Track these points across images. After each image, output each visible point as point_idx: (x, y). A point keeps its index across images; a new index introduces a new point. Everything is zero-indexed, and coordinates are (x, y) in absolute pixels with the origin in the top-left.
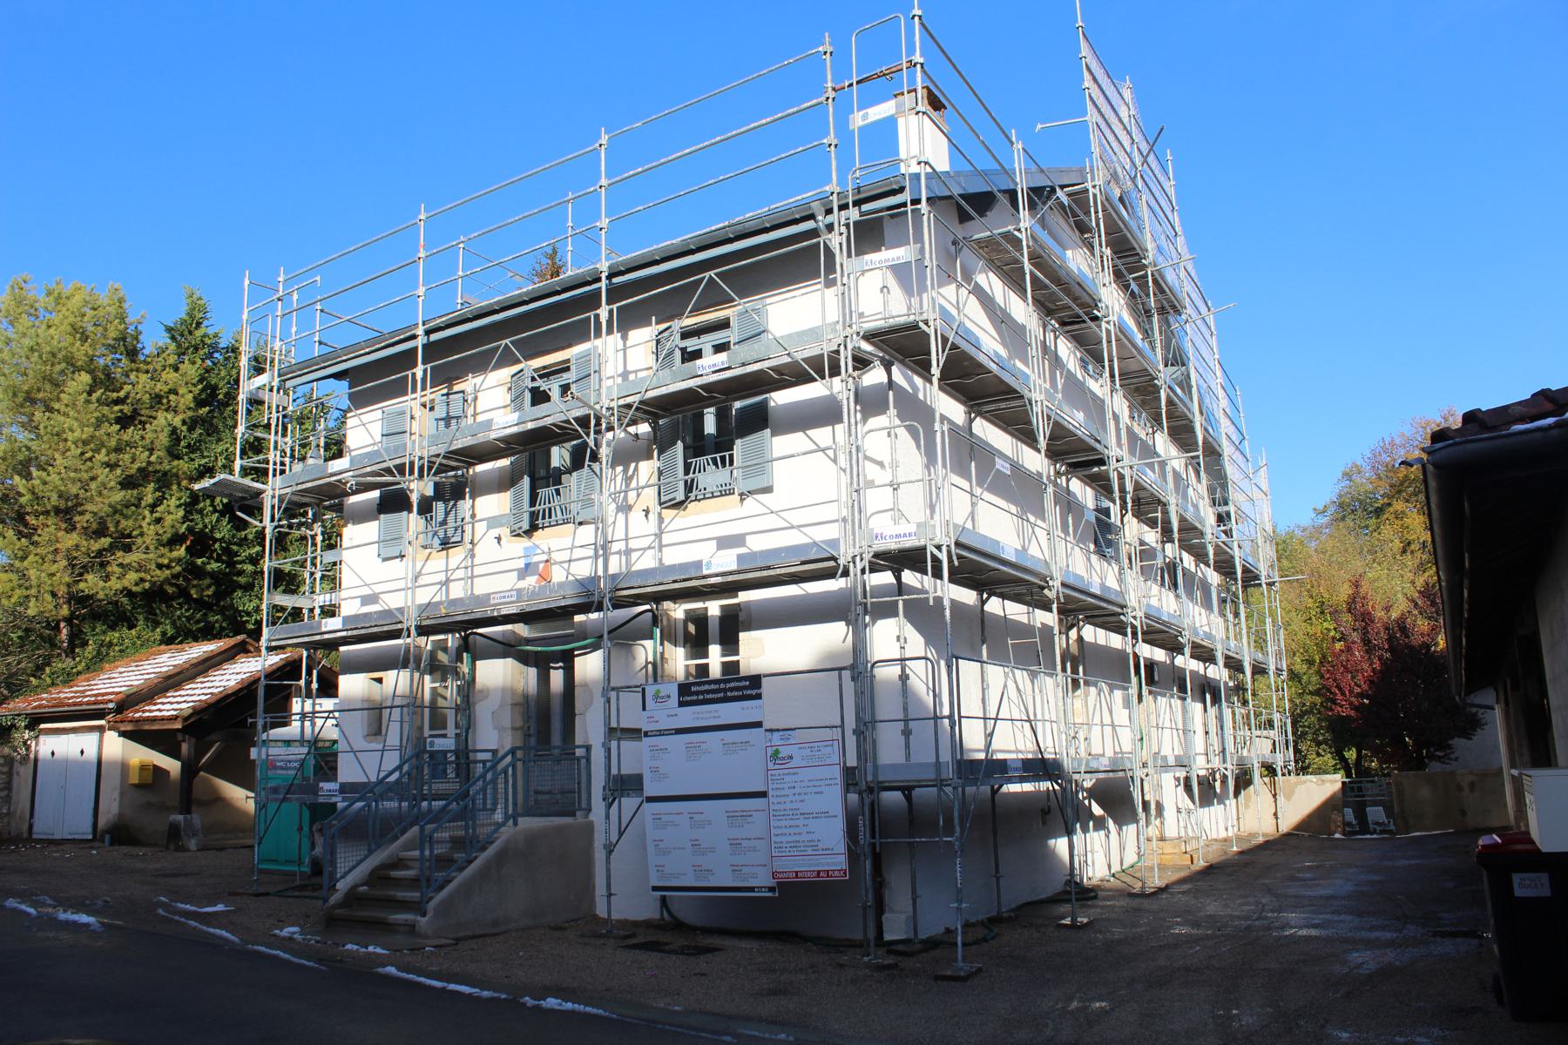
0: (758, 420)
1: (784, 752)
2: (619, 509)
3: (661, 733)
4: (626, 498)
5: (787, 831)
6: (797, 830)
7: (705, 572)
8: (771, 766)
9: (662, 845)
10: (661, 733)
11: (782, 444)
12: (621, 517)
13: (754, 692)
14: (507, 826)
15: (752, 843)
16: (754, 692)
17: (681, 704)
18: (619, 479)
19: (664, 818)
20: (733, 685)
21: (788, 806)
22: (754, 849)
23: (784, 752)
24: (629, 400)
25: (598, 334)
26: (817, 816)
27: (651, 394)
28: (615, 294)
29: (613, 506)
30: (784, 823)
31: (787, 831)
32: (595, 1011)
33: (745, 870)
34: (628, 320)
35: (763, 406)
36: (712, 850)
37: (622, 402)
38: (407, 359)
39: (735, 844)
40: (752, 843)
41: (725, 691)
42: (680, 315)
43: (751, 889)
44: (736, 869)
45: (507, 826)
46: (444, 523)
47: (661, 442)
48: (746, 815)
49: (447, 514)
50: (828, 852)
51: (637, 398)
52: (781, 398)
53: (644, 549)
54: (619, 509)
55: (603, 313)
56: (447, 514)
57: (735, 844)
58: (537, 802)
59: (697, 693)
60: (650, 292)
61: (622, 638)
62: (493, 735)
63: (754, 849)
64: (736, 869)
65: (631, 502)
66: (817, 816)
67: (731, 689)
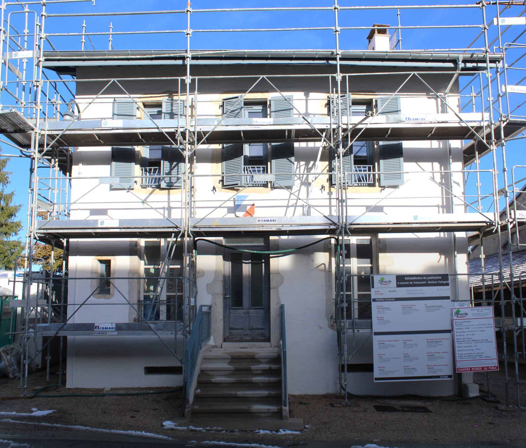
0: (396, 152)
1: (462, 311)
2: (302, 184)
3: (385, 300)
4: (307, 178)
5: (465, 349)
6: (471, 348)
7: (99, 226)
8: (455, 318)
9: (383, 357)
10: (385, 300)
11: (408, 166)
12: (304, 188)
13: (444, 282)
14: (216, 349)
15: (441, 355)
16: (444, 282)
17: (398, 286)
18: (302, 168)
19: (386, 343)
20: (431, 278)
21: (465, 337)
22: (442, 358)
23: (462, 311)
24: (54, 133)
25: (184, 90)
26: (482, 341)
27: (67, 132)
28: (344, 69)
29: (299, 182)
30: (461, 345)
31: (465, 349)
32: (163, 437)
33: (435, 368)
34: (206, 87)
35: (400, 146)
36: (417, 358)
37: (50, 133)
38: (181, 70)
39: (431, 356)
40: (441, 355)
41: (427, 280)
42: (244, 91)
43: (439, 377)
44: (429, 367)
45: (216, 349)
46: (169, 173)
47: (224, 157)
48: (438, 341)
49: (171, 169)
50: (488, 358)
51: (60, 133)
52: (407, 144)
53: (216, 208)
54: (302, 184)
55: (188, 79)
56: (171, 169)
57: (431, 356)
58: (231, 334)
59: (409, 281)
60: (226, 74)
61: (304, 251)
62: (208, 296)
63: (442, 358)
64: (429, 367)
65: (310, 180)
66: (482, 341)
67: (431, 280)
